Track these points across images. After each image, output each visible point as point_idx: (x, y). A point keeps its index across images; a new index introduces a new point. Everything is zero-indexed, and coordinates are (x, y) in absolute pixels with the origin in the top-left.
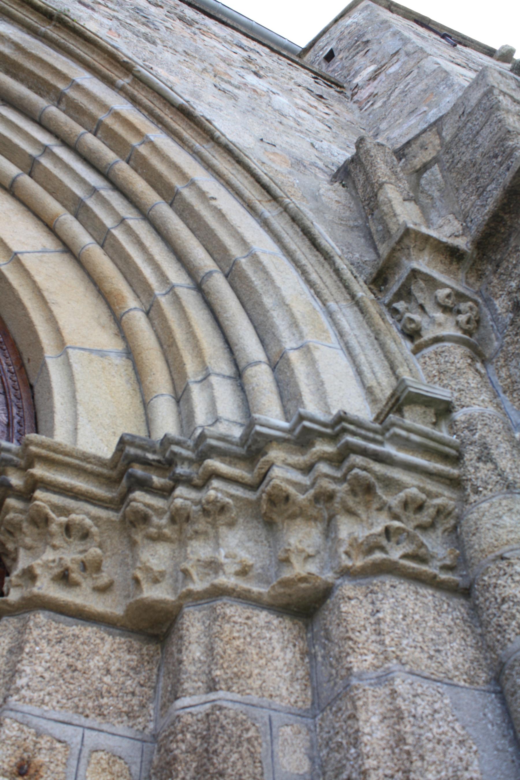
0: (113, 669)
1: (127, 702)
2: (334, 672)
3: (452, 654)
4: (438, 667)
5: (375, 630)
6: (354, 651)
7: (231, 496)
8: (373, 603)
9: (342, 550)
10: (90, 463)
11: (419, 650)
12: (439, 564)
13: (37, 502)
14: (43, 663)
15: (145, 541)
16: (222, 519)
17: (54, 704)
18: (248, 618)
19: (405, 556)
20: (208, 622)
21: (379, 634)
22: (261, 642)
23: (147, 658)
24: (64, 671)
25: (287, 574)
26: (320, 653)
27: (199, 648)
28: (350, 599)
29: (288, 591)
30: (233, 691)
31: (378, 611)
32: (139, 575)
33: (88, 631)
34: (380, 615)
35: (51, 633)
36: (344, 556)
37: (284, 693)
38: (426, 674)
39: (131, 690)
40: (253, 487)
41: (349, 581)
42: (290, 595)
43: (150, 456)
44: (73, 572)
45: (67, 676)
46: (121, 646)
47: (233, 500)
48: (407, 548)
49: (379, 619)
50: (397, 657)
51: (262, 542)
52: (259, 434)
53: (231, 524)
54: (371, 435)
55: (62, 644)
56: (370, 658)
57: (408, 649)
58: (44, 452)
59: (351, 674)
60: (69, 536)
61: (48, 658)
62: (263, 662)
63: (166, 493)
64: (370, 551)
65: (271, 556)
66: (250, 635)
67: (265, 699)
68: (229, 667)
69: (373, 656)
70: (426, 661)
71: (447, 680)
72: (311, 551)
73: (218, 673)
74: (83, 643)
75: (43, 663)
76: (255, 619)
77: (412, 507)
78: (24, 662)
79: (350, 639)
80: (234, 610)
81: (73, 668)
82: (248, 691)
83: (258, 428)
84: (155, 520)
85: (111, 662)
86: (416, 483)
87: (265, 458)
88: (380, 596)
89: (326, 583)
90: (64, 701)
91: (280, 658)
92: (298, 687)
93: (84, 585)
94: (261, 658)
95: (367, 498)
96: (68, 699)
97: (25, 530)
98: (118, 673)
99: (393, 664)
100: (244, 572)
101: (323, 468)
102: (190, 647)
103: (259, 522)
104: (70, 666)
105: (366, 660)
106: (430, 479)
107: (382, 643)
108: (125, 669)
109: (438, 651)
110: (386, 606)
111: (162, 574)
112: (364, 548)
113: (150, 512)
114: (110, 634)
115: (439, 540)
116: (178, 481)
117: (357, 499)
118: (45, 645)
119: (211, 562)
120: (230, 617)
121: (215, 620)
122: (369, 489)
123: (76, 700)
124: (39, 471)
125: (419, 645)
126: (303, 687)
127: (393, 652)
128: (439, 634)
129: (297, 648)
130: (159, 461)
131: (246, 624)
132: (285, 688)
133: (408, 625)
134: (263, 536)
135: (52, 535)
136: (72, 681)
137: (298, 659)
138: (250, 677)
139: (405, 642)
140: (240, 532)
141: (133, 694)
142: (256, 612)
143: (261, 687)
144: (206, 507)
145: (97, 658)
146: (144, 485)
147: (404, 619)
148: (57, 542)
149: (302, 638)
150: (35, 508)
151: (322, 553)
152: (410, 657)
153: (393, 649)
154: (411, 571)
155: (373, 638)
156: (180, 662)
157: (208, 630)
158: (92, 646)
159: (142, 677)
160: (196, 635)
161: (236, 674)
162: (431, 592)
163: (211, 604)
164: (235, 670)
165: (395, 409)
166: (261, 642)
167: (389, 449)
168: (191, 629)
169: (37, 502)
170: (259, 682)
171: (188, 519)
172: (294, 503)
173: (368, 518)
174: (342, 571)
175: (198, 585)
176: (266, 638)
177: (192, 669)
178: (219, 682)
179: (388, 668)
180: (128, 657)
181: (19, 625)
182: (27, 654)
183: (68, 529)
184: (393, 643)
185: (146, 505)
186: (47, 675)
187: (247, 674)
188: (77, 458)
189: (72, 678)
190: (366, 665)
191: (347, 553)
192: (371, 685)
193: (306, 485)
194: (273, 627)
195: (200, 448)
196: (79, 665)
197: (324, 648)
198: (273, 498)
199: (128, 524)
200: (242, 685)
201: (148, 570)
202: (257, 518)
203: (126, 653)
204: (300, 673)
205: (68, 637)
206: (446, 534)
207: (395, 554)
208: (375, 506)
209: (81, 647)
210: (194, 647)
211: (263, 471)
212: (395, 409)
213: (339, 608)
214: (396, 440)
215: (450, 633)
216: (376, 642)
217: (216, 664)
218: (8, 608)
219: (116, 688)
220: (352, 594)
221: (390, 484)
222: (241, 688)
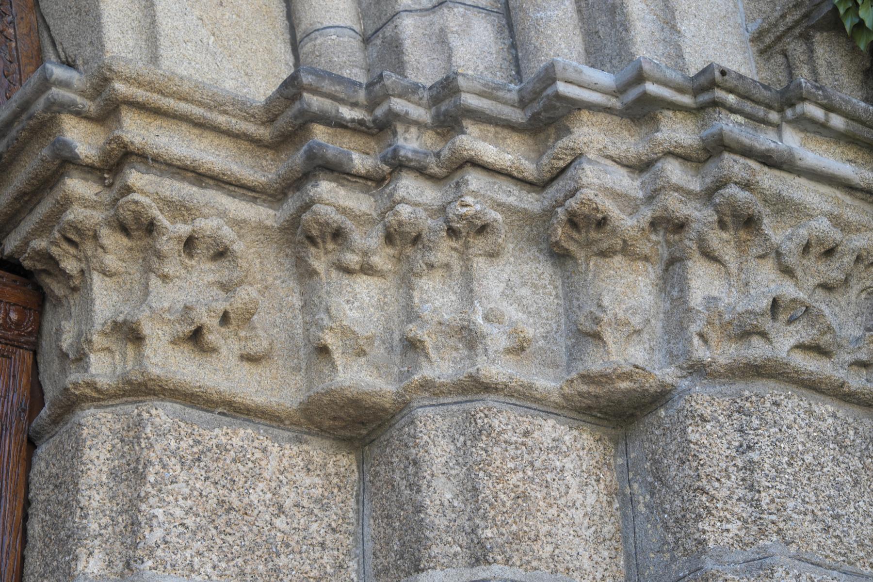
0: (288, 503)
1: (315, 561)
2: (670, 538)
3: (856, 521)
4: (835, 544)
5: (743, 480)
6: (710, 513)
7: (499, 206)
8: (741, 430)
9: (694, 328)
10: (225, 112)
11: (809, 517)
12: (848, 358)
13: (136, 197)
14: (181, 502)
15: (334, 273)
16: (479, 244)
17: (209, 570)
18: (526, 434)
19: (800, 347)
20: (462, 439)
21: (751, 488)
22: (549, 477)
23: (335, 480)
24: (214, 512)
25: (595, 364)
26: (643, 499)
27: (450, 485)
28: (704, 420)
29: (592, 389)
30: (513, 564)
31: (749, 447)
32: (329, 339)
33: (241, 436)
34: (755, 456)
35: (183, 445)
36: (696, 340)
37: (587, 564)
38: (819, 558)
39: (320, 539)
40: (538, 186)
41: (704, 386)
42: (596, 397)
43: (347, 113)
44: (210, 332)
45: (221, 522)
46: (294, 461)
47: (502, 212)
48: (802, 333)
49: (751, 462)
50: (779, 532)
51: (545, 287)
52: (558, 97)
53: (493, 255)
54: (761, 111)
55: (202, 464)
56: (734, 527)
57: (795, 516)
58: (141, 94)
59: (704, 552)
60: (191, 256)
61: (186, 491)
62: (553, 511)
63: (375, 182)
64: (745, 335)
65: (559, 314)
66: (532, 464)
67: (559, 575)
68: (504, 523)
69: (740, 523)
70: (820, 537)
71: (847, 567)
72: (636, 321)
73: (489, 533)
74: (234, 461)
75: (181, 502)
76: (536, 435)
77: (815, 250)
78: (152, 501)
79: (704, 491)
80: (504, 419)
81: (226, 506)
82: (535, 564)
83: (562, 88)
84: (357, 237)
85: (284, 490)
86: (827, 207)
87: (564, 142)
88: (756, 422)
89: (663, 385)
90: (223, 565)
91: (578, 505)
92: (606, 554)
93: (224, 351)
94: (551, 506)
95: (743, 235)
96: (228, 561)
97: (105, 241)
98: (295, 510)
99: (771, 541)
100: (519, 349)
101: (674, 171)
102: (434, 484)
103: (540, 251)
104: (221, 503)
105: (728, 530)
106: (851, 195)
107: (756, 504)
108: (305, 503)
109: (837, 517)
110: (764, 441)
111: (370, 339)
112: (733, 330)
113: (349, 224)
114: (275, 439)
115: (852, 310)
116: (398, 165)
117: (725, 235)
118: (178, 467)
119: (462, 328)
120: (499, 433)
121: (476, 438)
122: (749, 222)
123: (240, 561)
124: (135, 130)
125: (810, 508)
126: (613, 552)
127: (773, 523)
128: (839, 486)
129: (602, 486)
130: (361, 122)
131: (523, 444)
132: (587, 554)
133: (795, 474)
134: (546, 276)
135: (160, 256)
136: (228, 530)
137: (605, 504)
138: (537, 538)
139: (791, 504)
140: (508, 269)
141: (322, 545)
142: (539, 421)
143: (552, 557)
144: (455, 225)
145: (261, 486)
146: (338, 171)
147: (790, 464)
148: (169, 268)
149: (609, 465)
150: (133, 207)
151: (653, 321)
152: (798, 531)
153: (774, 517)
154: (806, 377)
155: (740, 492)
156: (419, 508)
157: (463, 453)
158: (250, 465)
159: (332, 517)
160: (443, 460)
161: (515, 535)
162: (830, 409)
163: (467, 406)
164: (514, 528)
165: (797, 31)
166: (549, 477)
167: (791, 141)
168: (433, 450)
169: (136, 197)
170: (549, 548)
171: (417, 239)
172: (614, 231)
173: (741, 270)
174: (692, 367)
175: (441, 367)
176: (555, 468)
177: (441, 522)
178: (491, 550)
179: (765, 548)
180: (308, 481)
181: (118, 426)
182: (153, 486)
183: (189, 244)
184: (773, 507)
185: (344, 211)
186: (190, 521)
187: (532, 535)
188: (200, 104)
189: (228, 524)
190: (727, 538)
191: (701, 336)
192: (735, 572)
193: (636, 199)
194: (564, 448)
195: (443, 107)
196: (233, 497)
197: (652, 495)
198: (576, 219)
199: (299, 237)
200: (525, 554)
201: (346, 332)
202: (538, 244)
203: (303, 474)
204: (608, 529)
205: (209, 450)
206: (863, 296)
207: (783, 343)
208: (756, 251)
209: (233, 467)
210: (440, 483)
211: (562, 164)
212: (797, 31)
213: (684, 431)
214: (804, 124)
215: (856, 483)
216: (746, 502)
217: (484, 518)
218: (95, 395)
219: (296, 537)
220: (707, 412)
221: (782, 206)
222: (525, 558)
